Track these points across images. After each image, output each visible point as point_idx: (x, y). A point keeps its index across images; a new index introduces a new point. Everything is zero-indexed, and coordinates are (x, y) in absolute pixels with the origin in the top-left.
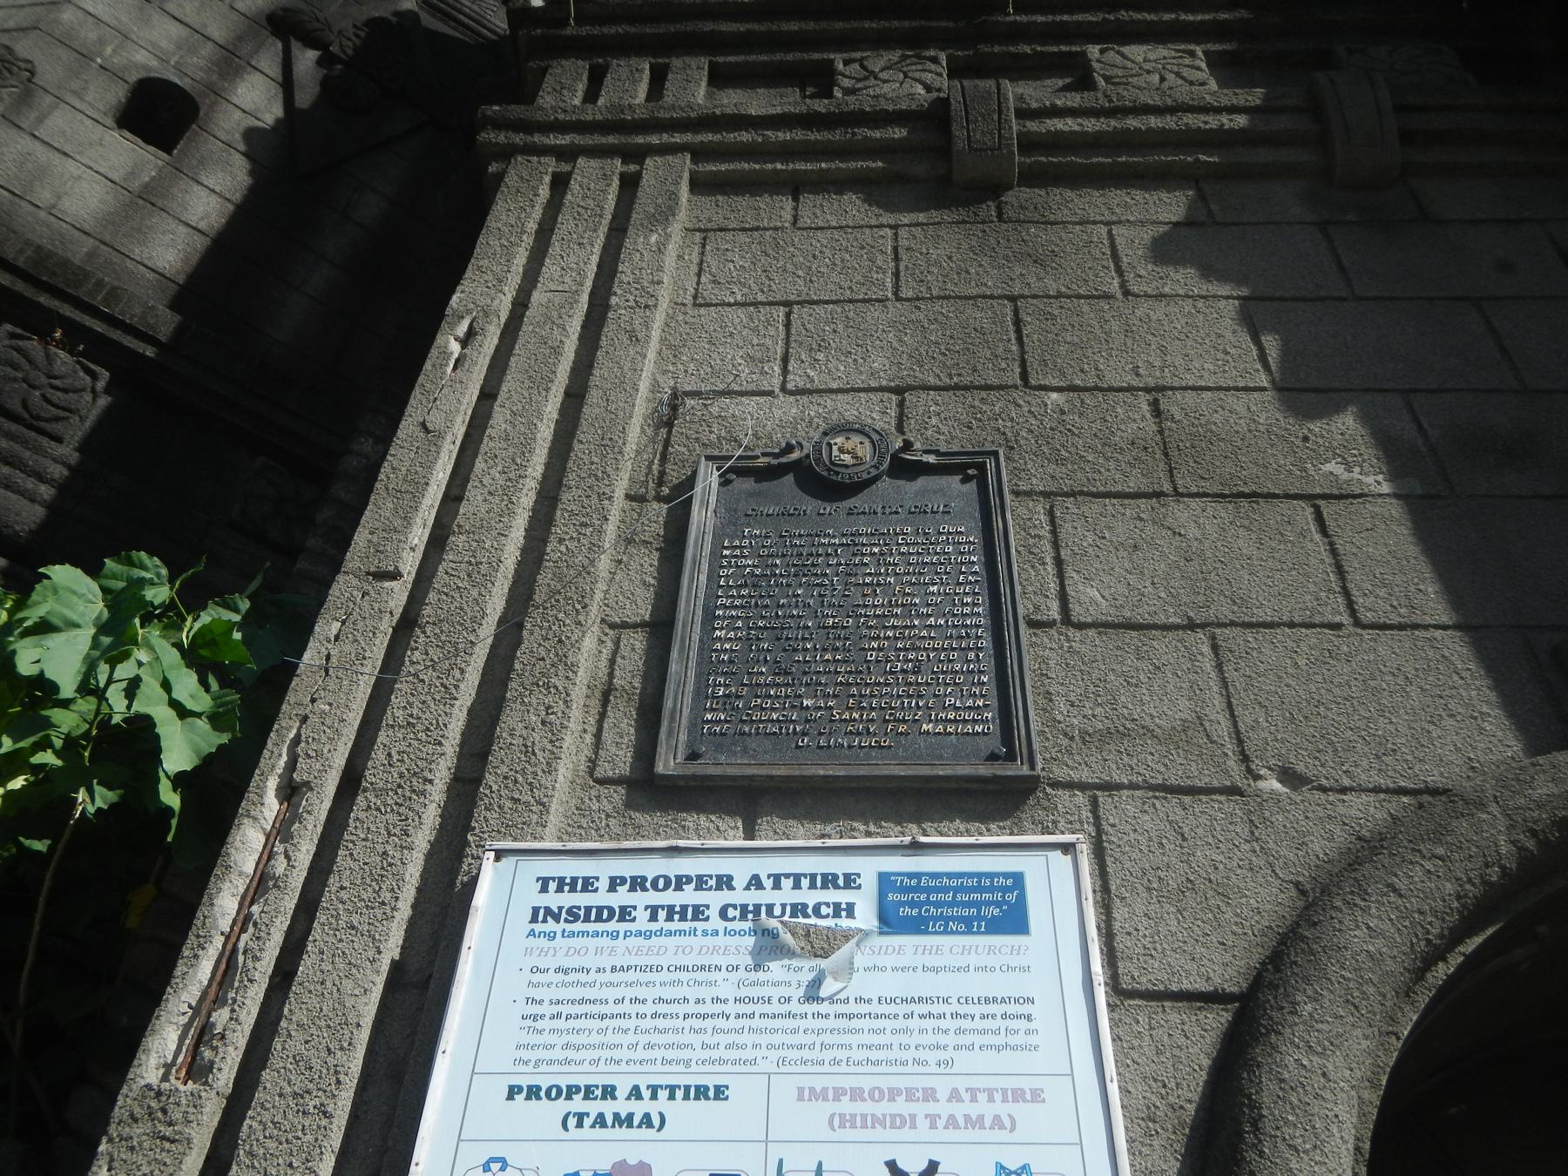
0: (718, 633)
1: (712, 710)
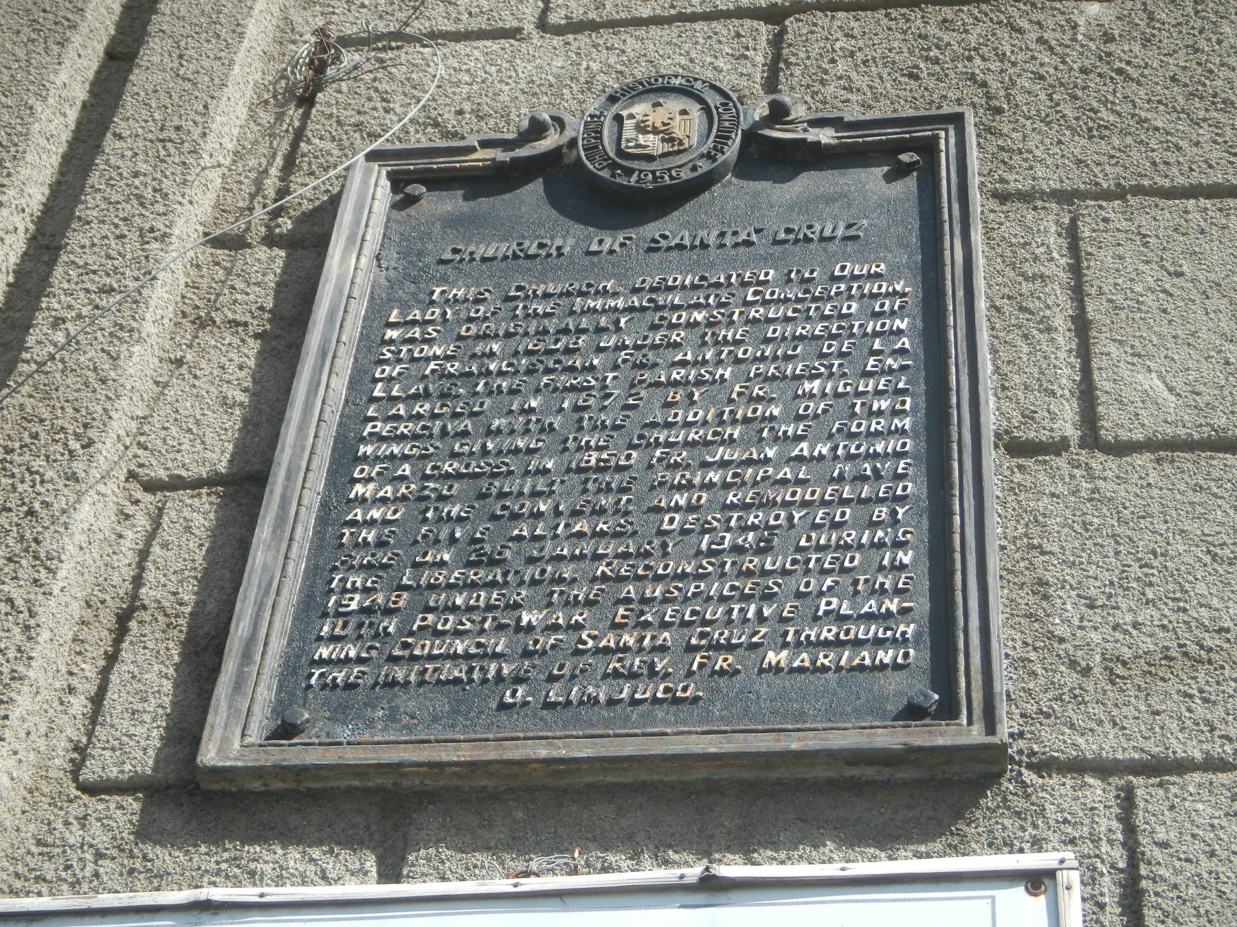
0: (359, 489)
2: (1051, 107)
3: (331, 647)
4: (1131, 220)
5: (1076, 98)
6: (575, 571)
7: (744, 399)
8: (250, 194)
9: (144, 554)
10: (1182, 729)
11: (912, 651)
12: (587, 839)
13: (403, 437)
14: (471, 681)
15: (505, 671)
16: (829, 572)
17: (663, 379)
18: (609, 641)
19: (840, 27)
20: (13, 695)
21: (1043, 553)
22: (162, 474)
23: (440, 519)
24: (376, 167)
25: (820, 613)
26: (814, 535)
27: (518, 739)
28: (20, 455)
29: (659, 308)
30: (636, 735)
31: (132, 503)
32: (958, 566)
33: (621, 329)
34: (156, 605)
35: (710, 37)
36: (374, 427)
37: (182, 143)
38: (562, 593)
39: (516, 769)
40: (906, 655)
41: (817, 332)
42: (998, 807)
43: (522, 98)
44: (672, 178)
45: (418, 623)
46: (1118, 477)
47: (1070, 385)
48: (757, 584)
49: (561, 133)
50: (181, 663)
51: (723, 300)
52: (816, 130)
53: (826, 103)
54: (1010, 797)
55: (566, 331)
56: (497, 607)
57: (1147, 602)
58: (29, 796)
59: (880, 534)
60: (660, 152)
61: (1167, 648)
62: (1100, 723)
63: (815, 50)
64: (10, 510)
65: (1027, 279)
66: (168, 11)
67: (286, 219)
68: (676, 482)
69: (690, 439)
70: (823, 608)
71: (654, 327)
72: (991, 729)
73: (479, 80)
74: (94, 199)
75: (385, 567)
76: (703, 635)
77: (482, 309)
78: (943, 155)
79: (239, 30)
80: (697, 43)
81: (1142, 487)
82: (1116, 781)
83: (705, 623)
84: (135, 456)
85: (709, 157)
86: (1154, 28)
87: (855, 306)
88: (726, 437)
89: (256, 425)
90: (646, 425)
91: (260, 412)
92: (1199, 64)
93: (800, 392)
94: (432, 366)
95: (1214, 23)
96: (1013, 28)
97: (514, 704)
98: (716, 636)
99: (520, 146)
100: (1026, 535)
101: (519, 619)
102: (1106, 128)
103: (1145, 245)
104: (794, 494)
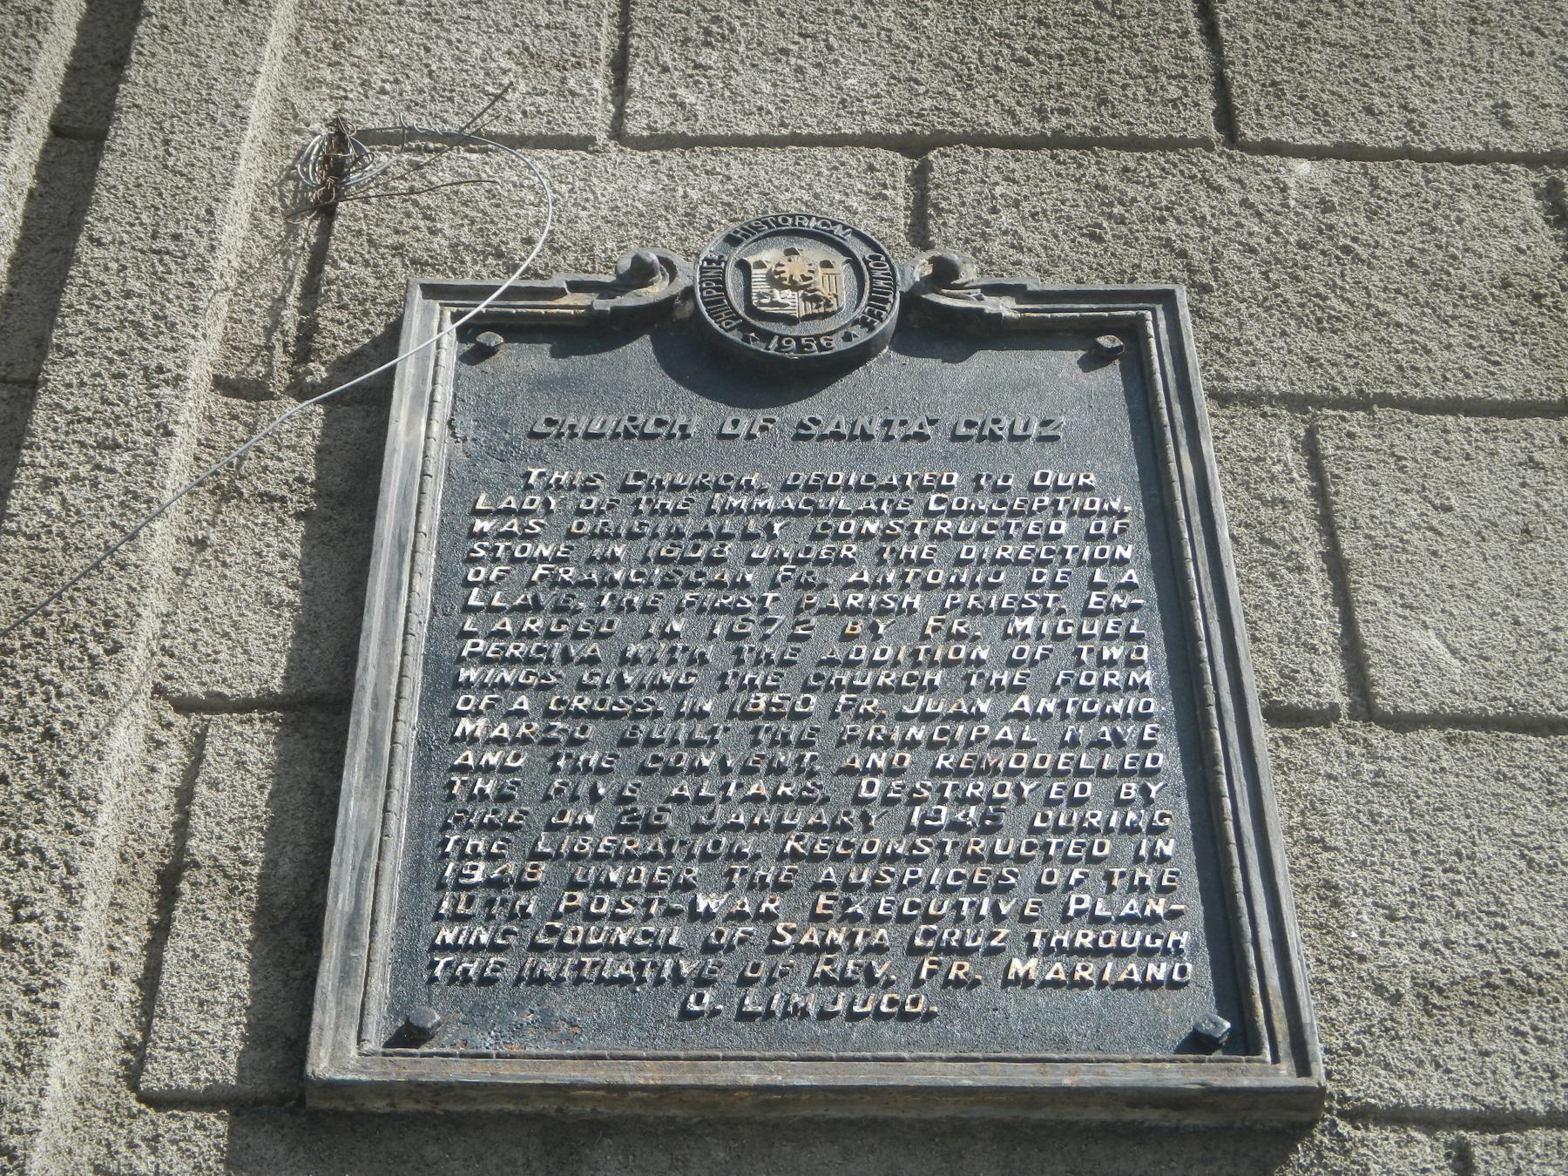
0: (466, 725)
2: (1269, 289)
4: (1380, 436)
5: (1297, 279)
6: (756, 845)
7: (942, 635)
8: (264, 327)
9: (184, 796)
10: (1518, 1075)
11: (1189, 966)
13: (513, 660)
14: (641, 981)
15: (685, 970)
16: (1076, 860)
17: (836, 604)
18: (811, 936)
19: (997, 168)
20: (61, 976)
21: (1327, 849)
22: (198, 690)
23: (575, 769)
24: (438, 307)
25: (1071, 913)
26: (1050, 814)
27: (716, 1058)
28: (22, 658)
29: (818, 513)
30: (865, 1059)
31: (163, 727)
32: (1236, 862)
33: (775, 536)
34: (211, 863)
35: (835, 168)
36: (475, 645)
37: (185, 257)
38: (744, 872)
39: (717, 1097)
40: (1183, 971)
41: (1021, 556)
42: (1312, 1164)
43: (606, 228)
44: (821, 348)
45: (564, 903)
46: (1405, 758)
47: (1331, 639)
48: (988, 873)
49: (672, 279)
50: (255, 940)
51: (900, 507)
52: (993, 299)
53: (991, 263)
54: (1326, 1153)
55: (705, 535)
56: (663, 887)
57: (1458, 917)
58: (79, 1108)
59: (1132, 816)
60: (803, 313)
61: (1489, 974)
62: (1420, 1063)
63: (970, 195)
64: (19, 730)
65: (1265, 503)
66: (140, 80)
67: (318, 365)
68: (870, 737)
69: (880, 683)
70: (1073, 907)
71: (816, 537)
72: (1303, 1068)
74: (74, 322)
75: (511, 828)
76: (928, 935)
77: (595, 500)
78: (1153, 341)
79: (240, 113)
80: (819, 174)
81: (1434, 772)
82: (1445, 1136)
83: (928, 919)
84: (161, 665)
85: (863, 322)
86: (1379, 198)
87: (1064, 525)
88: (925, 683)
89: (314, 633)
90: (821, 663)
91: (317, 616)
92: (1439, 247)
93: (1010, 631)
94: (540, 570)
95: (1450, 197)
96: (1210, 186)
97: (701, 1013)
98: (945, 936)
99: (623, 293)
100: (1303, 825)
101: (694, 904)
102: (1338, 319)
103: (1402, 469)
104: (1019, 760)
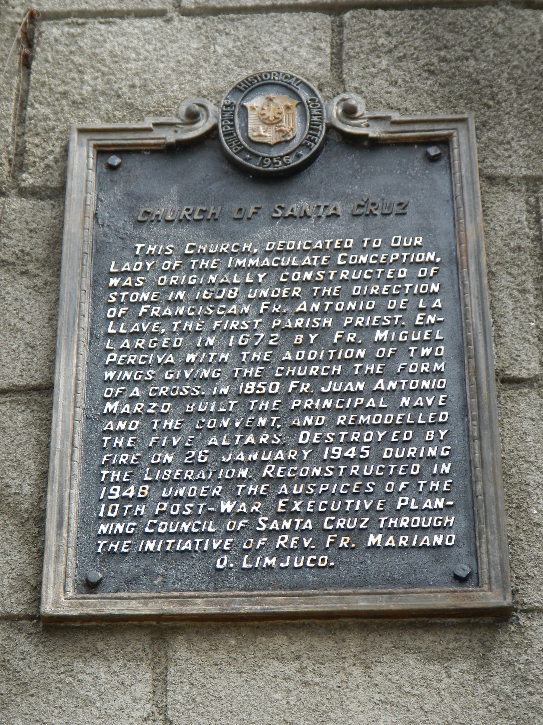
0: (109, 406)
1: (107, 519)
3: (108, 525)
12: (273, 658)
36: (112, 357)
73: (141, 57)
